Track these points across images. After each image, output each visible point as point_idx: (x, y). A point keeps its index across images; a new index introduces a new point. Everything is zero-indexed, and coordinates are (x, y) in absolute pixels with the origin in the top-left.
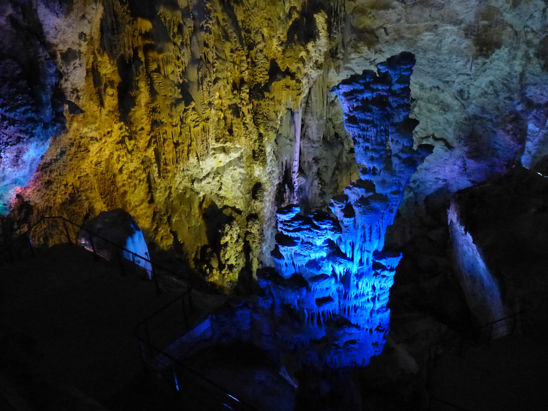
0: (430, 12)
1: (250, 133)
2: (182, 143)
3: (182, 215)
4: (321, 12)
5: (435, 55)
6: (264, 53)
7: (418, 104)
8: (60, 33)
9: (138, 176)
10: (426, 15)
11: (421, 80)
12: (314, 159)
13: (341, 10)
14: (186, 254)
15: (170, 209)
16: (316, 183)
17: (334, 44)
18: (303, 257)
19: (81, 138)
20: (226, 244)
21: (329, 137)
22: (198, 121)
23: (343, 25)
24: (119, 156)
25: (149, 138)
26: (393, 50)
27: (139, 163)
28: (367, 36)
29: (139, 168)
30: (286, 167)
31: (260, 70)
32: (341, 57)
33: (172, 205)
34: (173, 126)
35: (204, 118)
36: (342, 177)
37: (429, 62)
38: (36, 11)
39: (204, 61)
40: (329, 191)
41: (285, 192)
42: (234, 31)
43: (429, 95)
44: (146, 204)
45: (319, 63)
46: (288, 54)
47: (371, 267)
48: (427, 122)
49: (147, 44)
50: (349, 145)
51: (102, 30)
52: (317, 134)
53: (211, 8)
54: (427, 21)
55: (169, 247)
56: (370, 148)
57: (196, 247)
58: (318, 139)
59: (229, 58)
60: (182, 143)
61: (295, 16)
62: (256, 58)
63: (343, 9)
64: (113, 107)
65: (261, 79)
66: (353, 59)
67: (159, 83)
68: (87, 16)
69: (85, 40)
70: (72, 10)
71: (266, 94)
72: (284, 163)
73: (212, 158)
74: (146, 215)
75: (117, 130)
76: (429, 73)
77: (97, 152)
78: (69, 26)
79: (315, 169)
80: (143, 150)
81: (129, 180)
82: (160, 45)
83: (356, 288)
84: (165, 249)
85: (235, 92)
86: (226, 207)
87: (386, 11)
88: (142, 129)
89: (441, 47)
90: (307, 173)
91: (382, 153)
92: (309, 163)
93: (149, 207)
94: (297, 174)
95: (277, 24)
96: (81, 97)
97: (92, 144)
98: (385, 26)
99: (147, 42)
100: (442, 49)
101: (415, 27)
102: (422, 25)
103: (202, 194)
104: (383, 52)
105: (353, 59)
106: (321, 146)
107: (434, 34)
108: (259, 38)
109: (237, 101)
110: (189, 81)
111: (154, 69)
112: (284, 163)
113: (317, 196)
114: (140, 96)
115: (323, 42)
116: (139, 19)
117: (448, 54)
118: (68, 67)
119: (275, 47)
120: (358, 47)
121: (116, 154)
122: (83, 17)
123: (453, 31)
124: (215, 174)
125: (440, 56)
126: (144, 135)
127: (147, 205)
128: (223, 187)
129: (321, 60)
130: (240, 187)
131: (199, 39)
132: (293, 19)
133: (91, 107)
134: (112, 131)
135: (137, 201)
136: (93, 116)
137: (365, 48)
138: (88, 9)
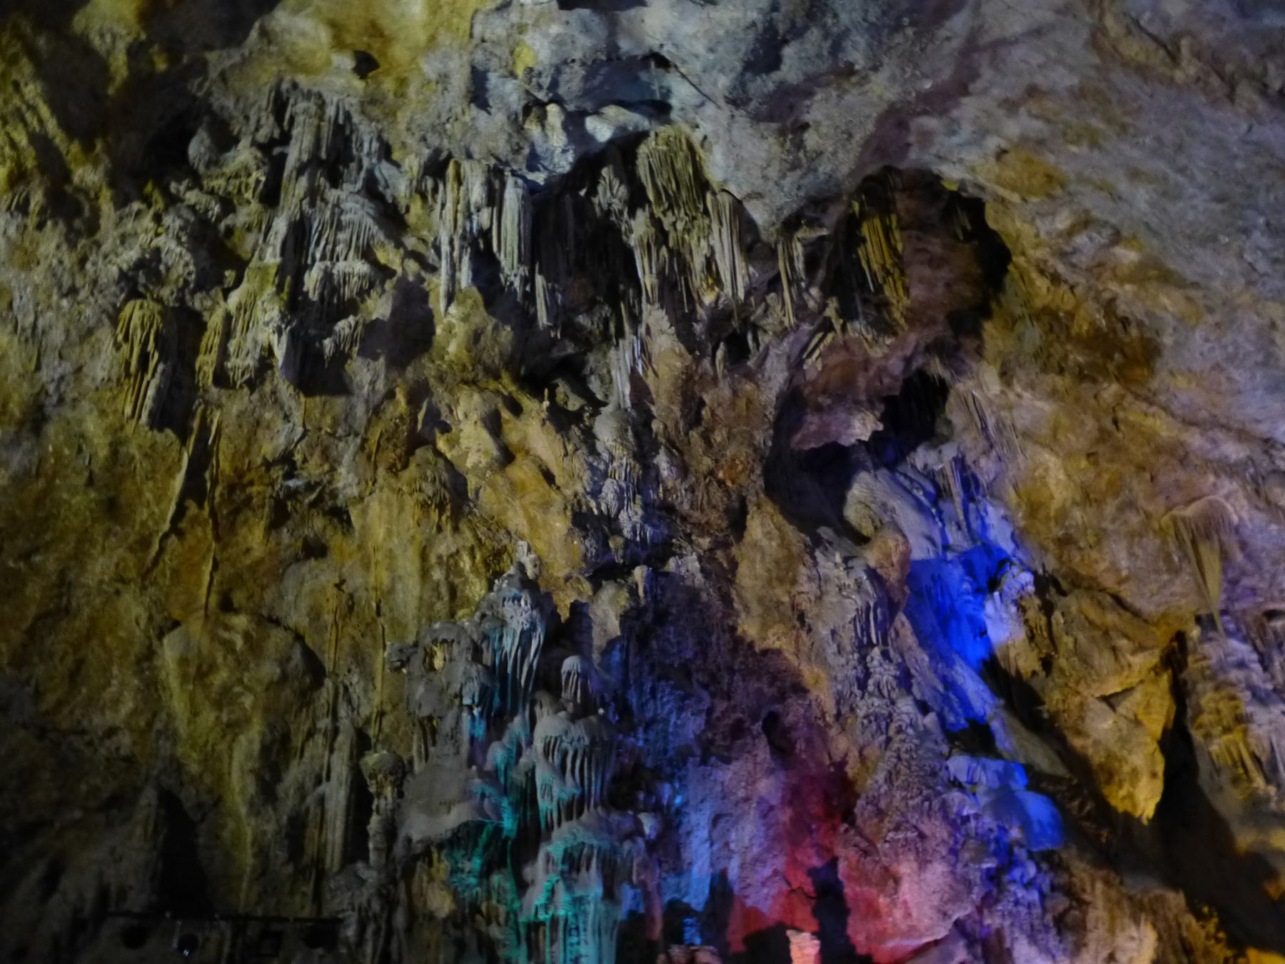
38: (1009, 952)
70: (1085, 945)
138: (1121, 940)
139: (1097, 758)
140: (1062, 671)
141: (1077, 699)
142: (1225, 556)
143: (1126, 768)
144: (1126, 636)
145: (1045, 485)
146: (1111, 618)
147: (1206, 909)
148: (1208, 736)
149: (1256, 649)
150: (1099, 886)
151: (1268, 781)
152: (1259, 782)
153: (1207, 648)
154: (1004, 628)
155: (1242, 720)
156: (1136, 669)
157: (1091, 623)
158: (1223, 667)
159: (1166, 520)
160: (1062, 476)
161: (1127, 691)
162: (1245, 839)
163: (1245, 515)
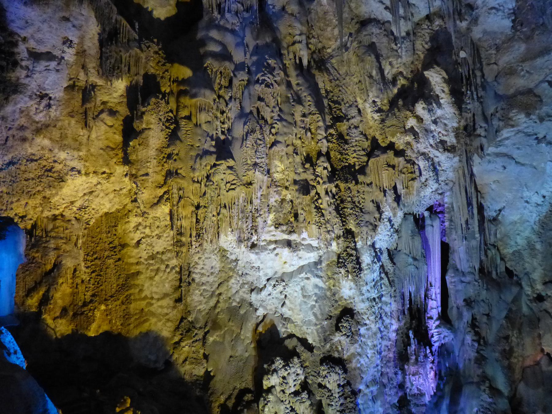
1: (328, 222)
2: (205, 207)
3: (227, 336)
4: (434, 68)
6: (361, 129)
9: (166, 260)
12: (465, 300)
14: (212, 393)
15: (213, 324)
16: (469, 338)
20: (270, 390)
21: (494, 273)
22: (234, 184)
23: (481, 93)
28: (524, 99)
30: (410, 300)
31: (353, 149)
32: (483, 134)
33: (217, 318)
34: (194, 181)
35: (245, 182)
39: (256, 116)
40: (493, 355)
41: (410, 345)
42: (310, 95)
44: (167, 302)
46: (388, 123)
49: (181, 90)
52: (468, 261)
53: (276, 66)
55: (195, 378)
57: (231, 387)
59: (299, 123)
60: (205, 207)
61: (401, 82)
62: (348, 134)
63: (478, 74)
65: (356, 160)
67: (187, 131)
69: (70, 46)
71: (361, 178)
72: (407, 295)
73: (272, 255)
74: (167, 317)
77: (85, 194)
79: (467, 316)
82: (194, 91)
84: (187, 377)
85: (307, 166)
86: (291, 336)
88: (147, 174)
90: (456, 324)
92: (458, 308)
93: (174, 307)
94: (437, 323)
95: (368, 84)
96: (54, 107)
103: (261, 312)
105: (507, 138)
108: (353, 112)
109: (309, 176)
110: (233, 138)
111: (183, 116)
112: (407, 295)
113: (473, 362)
118: (35, 64)
119: (371, 117)
124: (277, 281)
127: (171, 303)
128: (287, 302)
129: (451, 140)
130: (313, 307)
131: (252, 93)
132: (399, 86)
135: (156, 293)
137: (522, 117)
147: (155, 40)
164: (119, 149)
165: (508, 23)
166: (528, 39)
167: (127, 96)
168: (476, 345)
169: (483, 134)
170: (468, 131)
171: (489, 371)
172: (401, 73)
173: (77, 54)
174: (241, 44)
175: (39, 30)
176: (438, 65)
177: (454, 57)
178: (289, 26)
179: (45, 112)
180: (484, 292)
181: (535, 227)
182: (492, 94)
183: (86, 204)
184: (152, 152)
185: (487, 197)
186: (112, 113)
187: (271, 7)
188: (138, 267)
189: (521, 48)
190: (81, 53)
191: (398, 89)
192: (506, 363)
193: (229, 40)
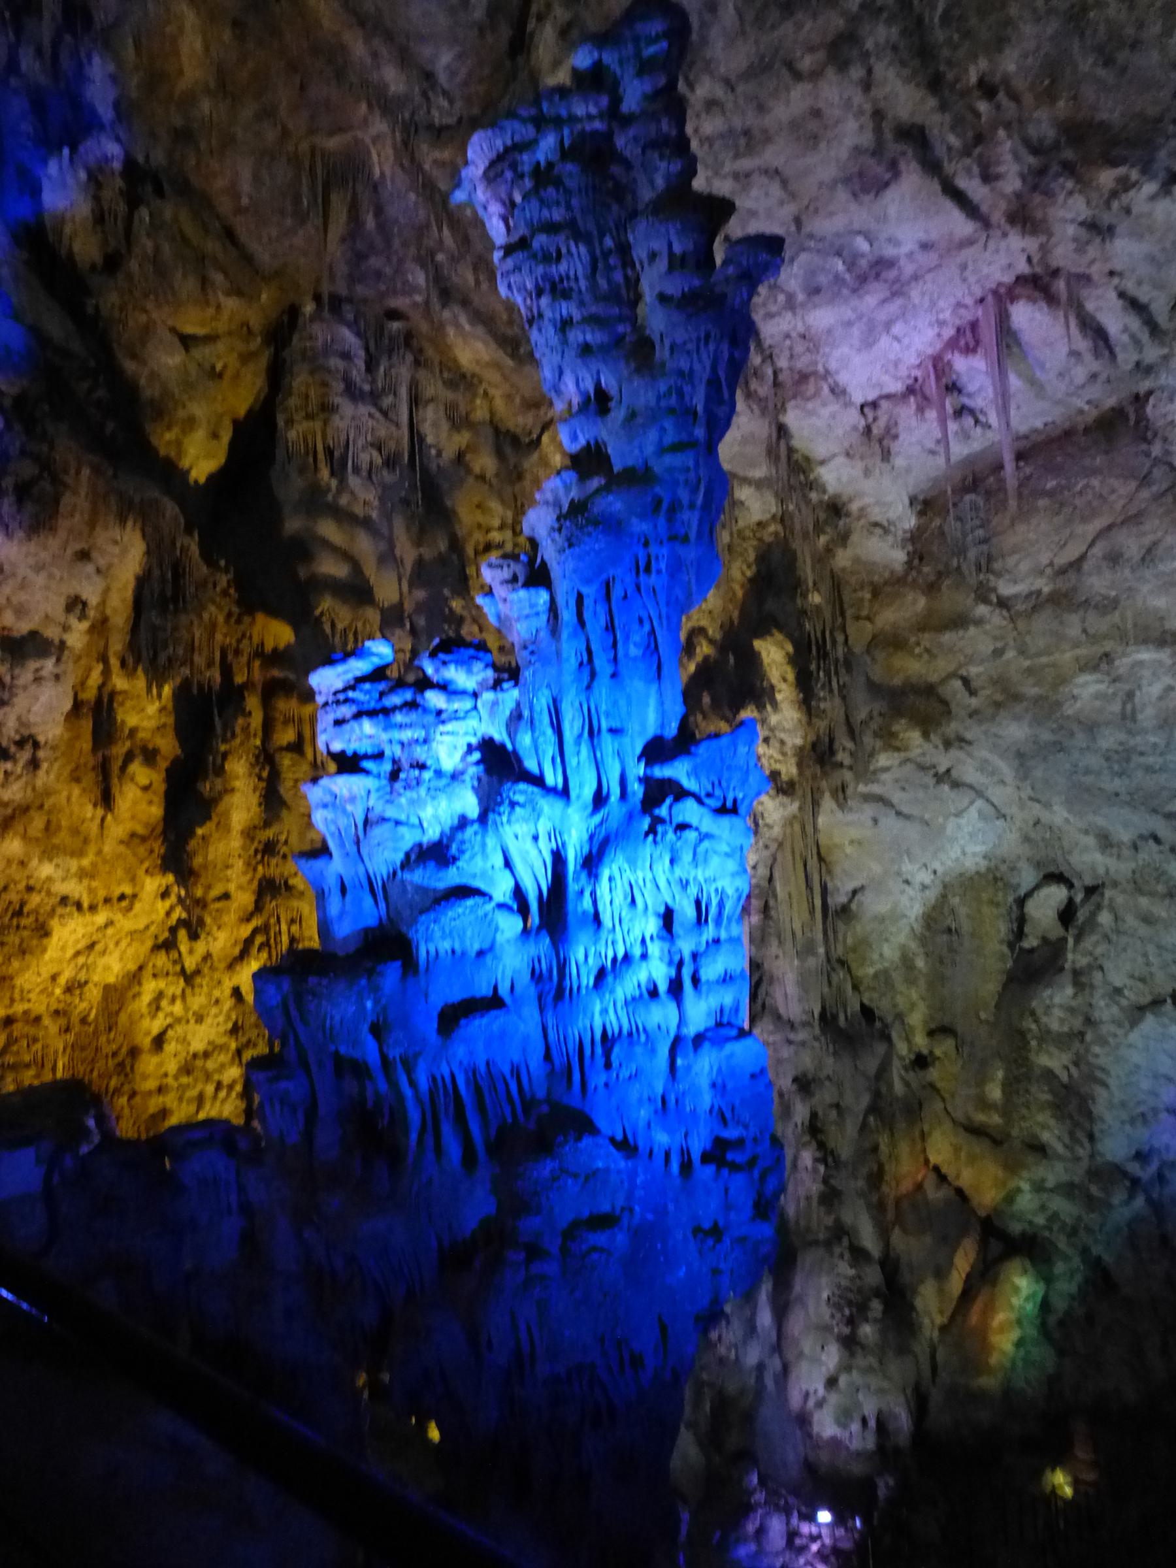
0: (1083, 621)
4: (772, 635)
5: (1122, 736)
7: (1106, 902)
8: (11, 582)
10: (1074, 631)
11: (1100, 821)
12: (795, 1080)
13: (834, 642)
17: (822, 725)
18: (390, 825)
19: (30, 889)
21: (842, 1018)
23: (845, 678)
24: (160, 995)
25: (246, 931)
26: (996, 735)
27: (222, 1029)
29: (222, 1048)
32: (847, 761)
36: (893, 1144)
37: (1108, 759)
40: (852, 1184)
43: (1133, 865)
45: (784, 777)
47: (639, 806)
48: (1145, 955)
50: (908, 1040)
51: (138, 604)
53: (465, 613)
54: (1076, 645)
56: (577, 315)
58: (804, 1018)
61: (704, 649)
63: (840, 638)
64: (146, 825)
66: (886, 769)
68: (94, 554)
69: (82, 617)
75: (154, 900)
76: (1117, 795)
77: (78, 954)
78: (39, 568)
79: (801, 1112)
80: (222, 965)
81: (185, 1080)
83: (591, 928)
87: (961, 633)
88: (226, 896)
89: (1134, 711)
91: (621, 329)
96: (45, 766)
97: (62, 916)
98: (963, 672)
99: (276, 673)
100: (1140, 717)
101: (1048, 666)
102: (1067, 657)
104: (970, 743)
105: (886, 769)
106: (816, 1039)
107: (1107, 679)
111: (284, 743)
113: (815, 1203)
114: (227, 799)
115: (785, 717)
116: (260, 618)
117: (1161, 727)
118: (17, 671)
120: (893, 735)
121: (150, 987)
122: (84, 556)
123: (1160, 662)
125: (1139, 739)
126: (231, 917)
129: (789, 770)
132: (699, 658)
133: (79, 805)
134: (135, 896)
136: (75, 831)
137: (915, 736)
138: (102, 537)
139: (149, 392)
140: (129, 277)
141: (143, 318)
142: (354, 217)
143: (181, 414)
144: (226, 274)
145: (177, 53)
146: (212, 246)
147: (222, 563)
148: (290, 422)
149: (367, 349)
150: (86, 472)
151: (332, 474)
152: (325, 473)
153: (317, 329)
154: (64, 194)
155: (328, 409)
156: (226, 315)
157: (184, 239)
158: (327, 351)
159: (304, 146)
160: (198, 45)
161: (210, 339)
162: (293, 525)
163: (388, 172)
164: (156, 839)
165: (898, 557)
166: (931, 589)
167: (175, 707)
168: (822, 1168)
169: (847, 761)
170: (819, 755)
171: (847, 1218)
172: (702, 631)
173: (92, 630)
174: (388, 557)
175: (24, 585)
176: (781, 629)
177: (799, 601)
178: (479, 506)
179: (24, 779)
180: (830, 1061)
181: (915, 926)
182: (862, 680)
183: (82, 977)
184: (236, 842)
185: (837, 870)
186: (150, 756)
187: (433, 452)
188: (161, 1099)
189: (916, 603)
190: (101, 627)
191: (698, 666)
192: (875, 1199)
193: (365, 546)
